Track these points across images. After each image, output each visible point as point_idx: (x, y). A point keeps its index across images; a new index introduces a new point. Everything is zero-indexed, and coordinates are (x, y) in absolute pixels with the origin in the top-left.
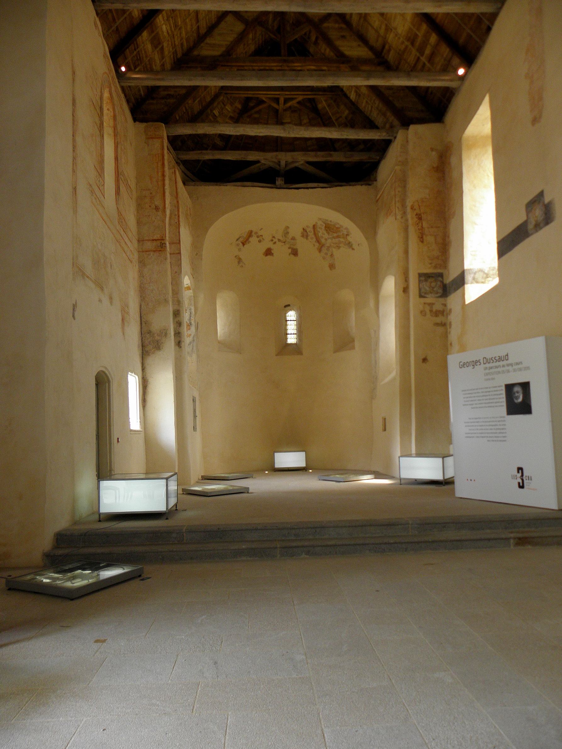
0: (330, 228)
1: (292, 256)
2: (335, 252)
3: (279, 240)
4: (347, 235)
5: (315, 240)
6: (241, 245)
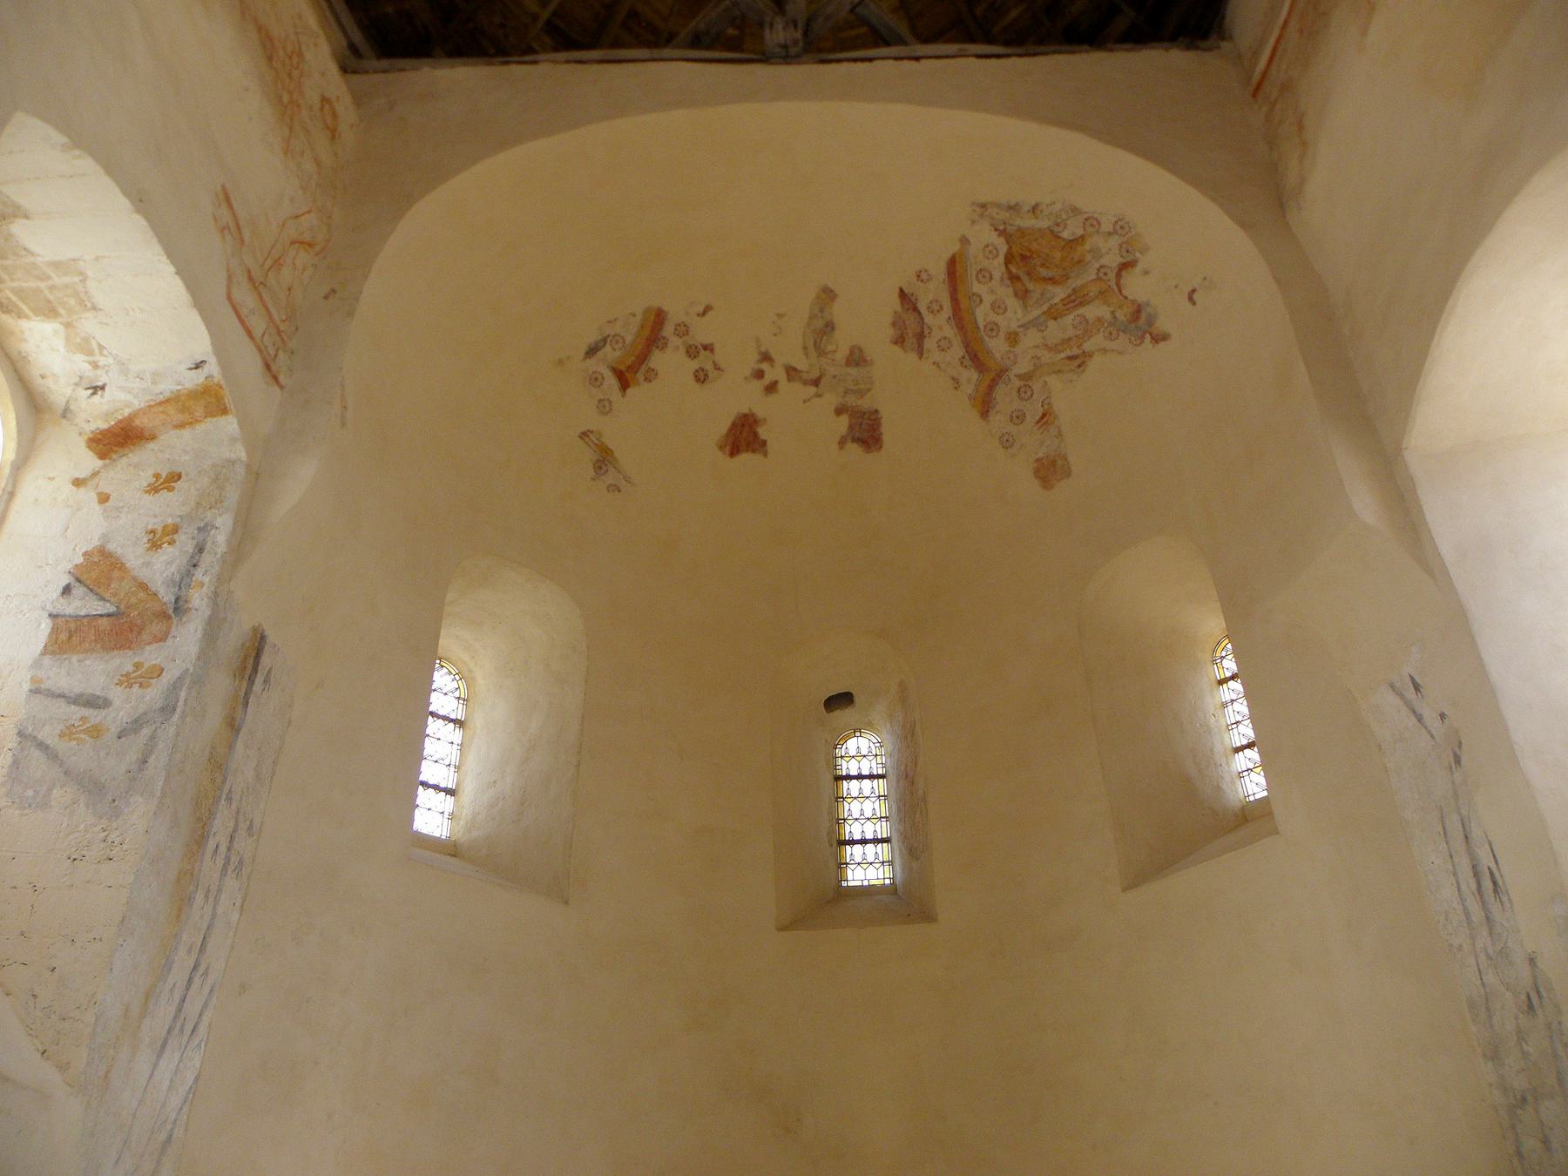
0: (1037, 255)
1: (854, 449)
2: (1064, 394)
3: (792, 372)
4: (1125, 266)
5: (958, 350)
6: (611, 381)
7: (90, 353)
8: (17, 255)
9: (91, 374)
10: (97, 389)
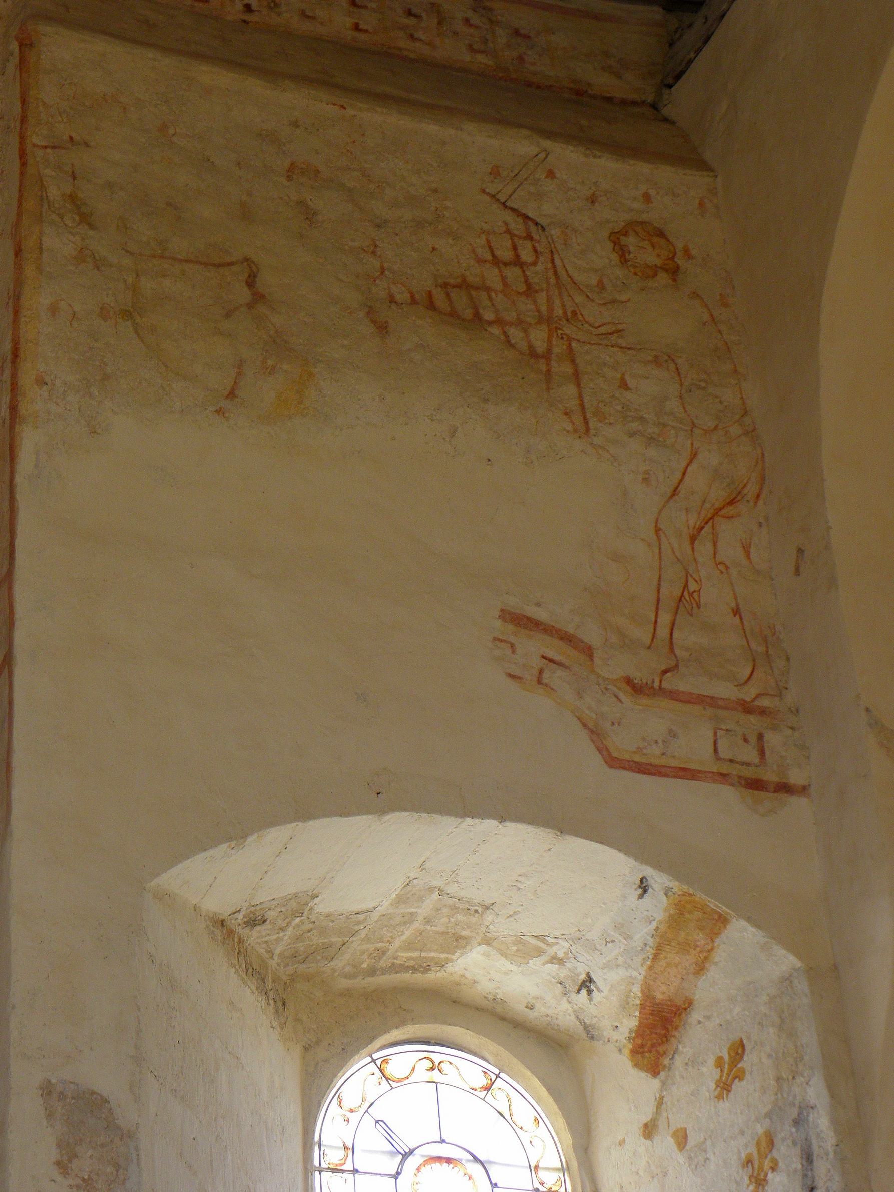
7: (540, 952)
8: (358, 923)
10: (587, 984)
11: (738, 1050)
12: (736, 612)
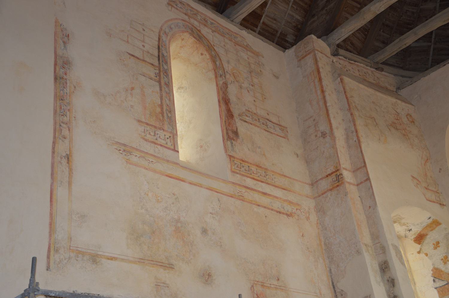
9: (407, 228)
10: (410, 230)
11: (438, 243)
12: (431, 177)
